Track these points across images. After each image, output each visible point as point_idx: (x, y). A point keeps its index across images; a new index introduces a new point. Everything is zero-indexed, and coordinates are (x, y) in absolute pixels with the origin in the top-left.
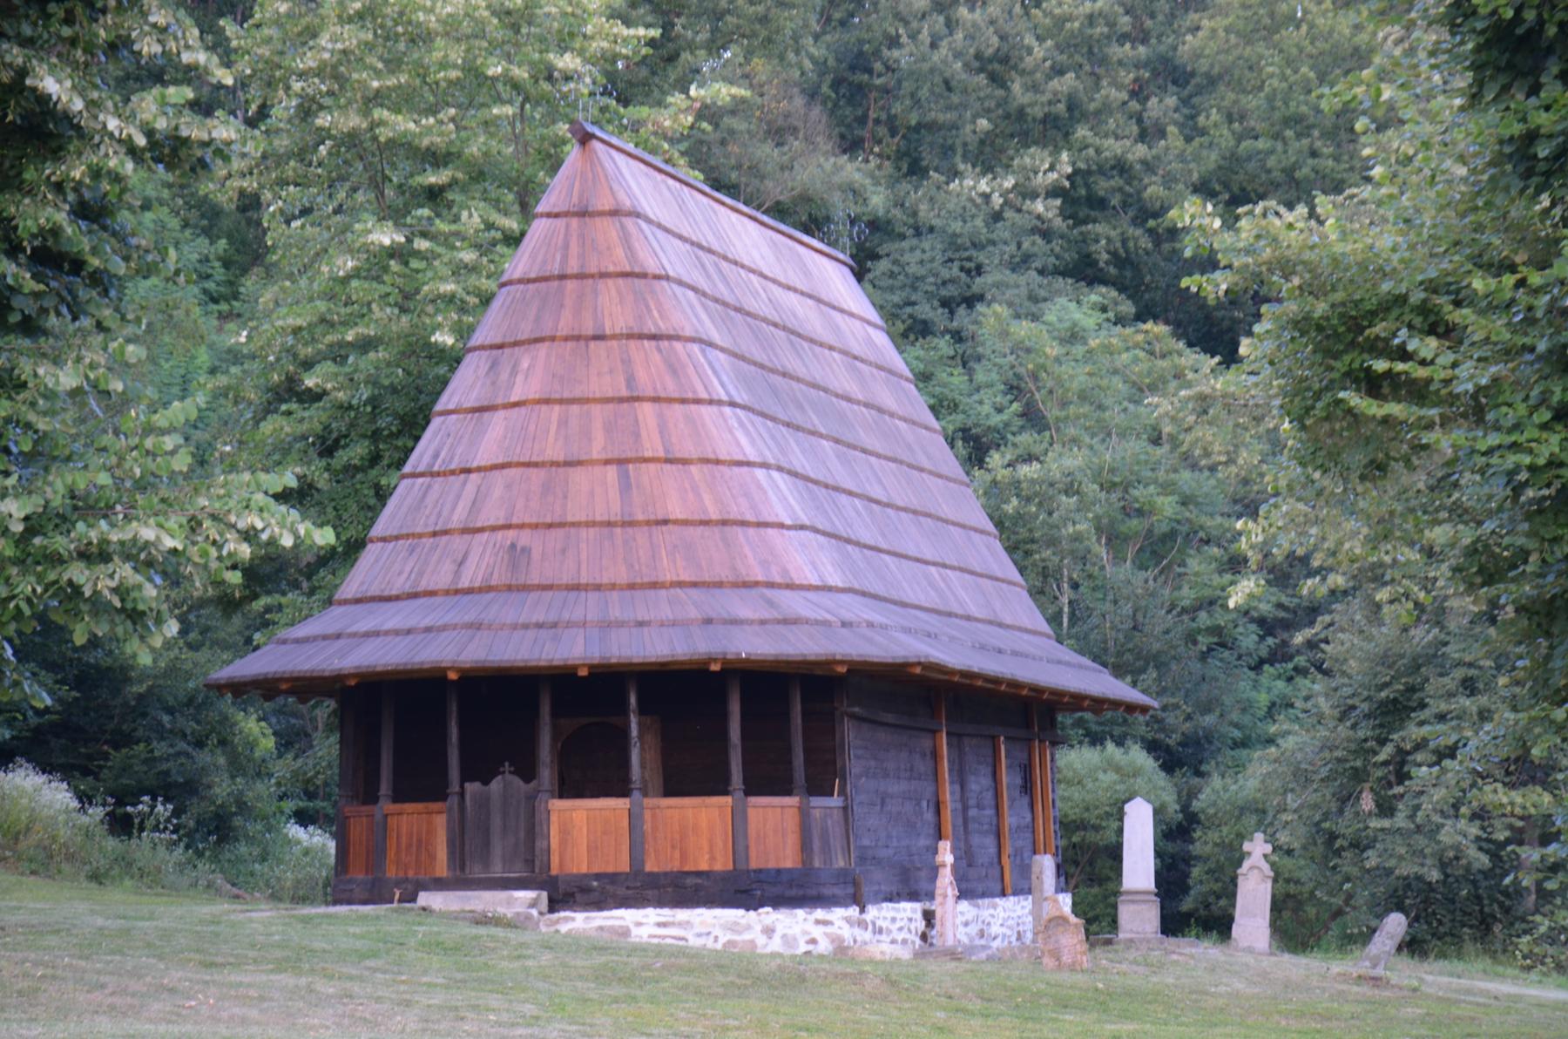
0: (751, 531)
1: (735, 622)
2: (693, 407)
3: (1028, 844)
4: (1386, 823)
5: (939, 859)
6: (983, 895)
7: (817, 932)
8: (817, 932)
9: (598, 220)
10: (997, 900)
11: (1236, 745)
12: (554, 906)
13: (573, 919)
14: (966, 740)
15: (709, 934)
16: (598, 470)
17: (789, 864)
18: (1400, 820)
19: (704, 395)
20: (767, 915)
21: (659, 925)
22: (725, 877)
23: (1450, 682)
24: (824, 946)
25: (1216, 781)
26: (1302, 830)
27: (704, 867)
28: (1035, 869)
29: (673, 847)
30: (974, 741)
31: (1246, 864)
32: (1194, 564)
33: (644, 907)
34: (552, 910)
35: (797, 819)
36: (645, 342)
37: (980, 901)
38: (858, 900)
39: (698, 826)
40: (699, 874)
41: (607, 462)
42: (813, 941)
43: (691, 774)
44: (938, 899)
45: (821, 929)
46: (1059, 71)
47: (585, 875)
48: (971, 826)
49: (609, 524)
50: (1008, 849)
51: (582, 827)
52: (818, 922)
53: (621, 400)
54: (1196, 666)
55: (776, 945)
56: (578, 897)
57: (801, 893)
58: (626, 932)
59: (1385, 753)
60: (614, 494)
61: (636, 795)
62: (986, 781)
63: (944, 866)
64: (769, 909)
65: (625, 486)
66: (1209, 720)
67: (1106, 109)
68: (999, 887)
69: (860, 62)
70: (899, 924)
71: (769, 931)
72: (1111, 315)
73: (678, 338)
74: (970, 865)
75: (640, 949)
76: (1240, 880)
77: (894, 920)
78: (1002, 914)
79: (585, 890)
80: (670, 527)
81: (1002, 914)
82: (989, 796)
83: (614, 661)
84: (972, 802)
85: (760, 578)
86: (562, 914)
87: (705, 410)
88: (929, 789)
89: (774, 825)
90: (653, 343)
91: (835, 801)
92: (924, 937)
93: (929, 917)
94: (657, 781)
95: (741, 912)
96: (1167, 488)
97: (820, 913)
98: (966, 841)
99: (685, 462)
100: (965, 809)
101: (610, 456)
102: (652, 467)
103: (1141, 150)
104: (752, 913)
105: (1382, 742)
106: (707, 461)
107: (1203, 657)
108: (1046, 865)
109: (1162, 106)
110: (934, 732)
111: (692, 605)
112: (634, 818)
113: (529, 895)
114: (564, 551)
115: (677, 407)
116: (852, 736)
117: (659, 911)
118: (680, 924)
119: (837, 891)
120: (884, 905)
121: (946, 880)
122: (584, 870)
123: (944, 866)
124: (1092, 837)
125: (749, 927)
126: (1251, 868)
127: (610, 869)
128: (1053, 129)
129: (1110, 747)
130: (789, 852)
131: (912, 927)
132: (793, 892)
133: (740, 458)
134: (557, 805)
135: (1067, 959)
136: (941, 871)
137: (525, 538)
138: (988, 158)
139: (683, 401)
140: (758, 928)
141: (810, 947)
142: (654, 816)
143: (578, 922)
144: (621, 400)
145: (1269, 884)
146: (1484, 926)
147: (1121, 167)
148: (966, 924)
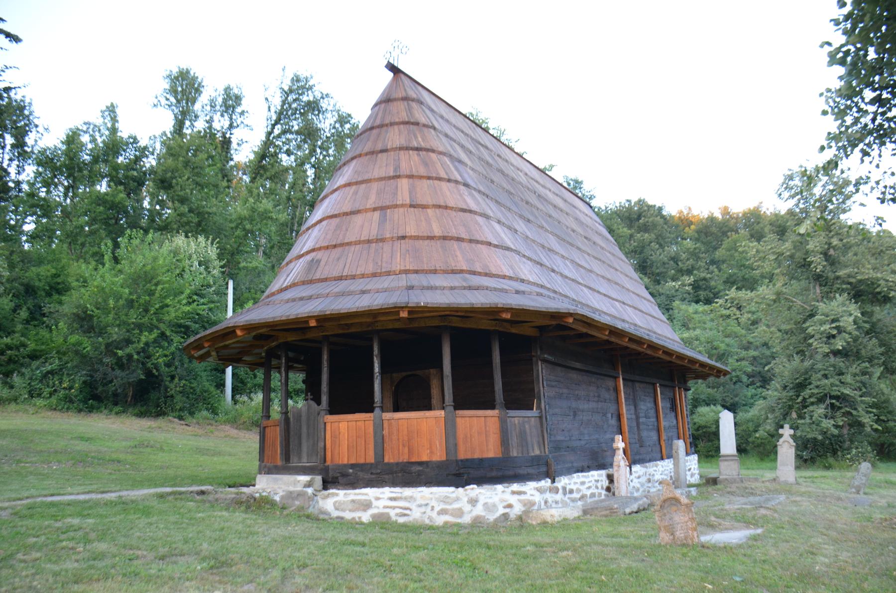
0: (465, 245)
1: (431, 288)
2: (436, 182)
3: (675, 434)
4: (803, 421)
5: (615, 445)
6: (650, 461)
7: (513, 500)
8: (513, 500)
9: (395, 103)
10: (658, 462)
11: (744, 405)
12: (327, 484)
13: (337, 495)
14: (637, 385)
15: (427, 505)
16: (369, 214)
17: (491, 455)
18: (808, 421)
19: (443, 174)
20: (473, 490)
21: (391, 499)
22: (440, 465)
23: (819, 375)
25: (741, 414)
26: (773, 425)
27: (425, 458)
28: (674, 447)
29: (404, 446)
30: (642, 385)
31: (781, 440)
32: (730, 360)
33: (383, 487)
34: (325, 488)
35: (497, 425)
36: (411, 152)
37: (647, 464)
38: (552, 475)
39: (423, 430)
40: (420, 463)
41: (375, 209)
42: (510, 506)
43: (411, 396)
44: (615, 468)
45: (517, 497)
46: (688, 259)
47: (345, 466)
48: (641, 427)
49: (369, 242)
50: (664, 436)
52: (513, 493)
53: (390, 178)
54: (732, 386)
55: (479, 510)
56: (341, 480)
57: (500, 474)
58: (367, 505)
59: (799, 400)
60: (375, 225)
61: (377, 411)
62: (650, 405)
63: (619, 449)
64: (475, 486)
65: (383, 221)
66: (737, 399)
67: (700, 267)
68: (659, 455)
69: (645, 261)
70: (587, 485)
71: (473, 502)
73: (433, 151)
74: (641, 446)
76: (779, 447)
77: (583, 483)
78: (661, 469)
79: (345, 475)
80: (407, 240)
81: (661, 469)
82: (652, 413)
83: (328, 313)
84: (642, 415)
85: (464, 268)
86: (331, 491)
87: (444, 185)
88: (612, 408)
89: (481, 430)
90: (416, 152)
91: (535, 412)
92: (608, 489)
93: (610, 478)
94: (389, 403)
95: (452, 489)
96: (722, 342)
97: (515, 487)
98: (639, 434)
99: (424, 207)
100: (638, 418)
101: (377, 205)
102: (401, 210)
103: (709, 276)
104: (460, 489)
105: (798, 396)
106: (440, 207)
107: (735, 383)
108: (680, 445)
109: (713, 268)
110: (616, 378)
112: (379, 427)
113: (304, 478)
114: (338, 259)
115: (426, 183)
116: (542, 371)
117: (393, 489)
118: (406, 499)
119: (530, 471)
120: (575, 475)
121: (620, 459)
122: (345, 462)
123: (619, 449)
124: (709, 430)
125: (457, 499)
126: (784, 442)
127: (362, 461)
128: (689, 272)
129: (712, 406)
130: (491, 447)
131: (599, 485)
132: (494, 474)
133: (465, 207)
134: (330, 418)
135: (680, 534)
136: (617, 452)
138: (673, 280)
139: (429, 178)
140: (466, 499)
141: (507, 510)
142: (390, 425)
143: (337, 502)
144: (390, 178)
145: (793, 450)
146: (834, 453)
147: (705, 279)
148: (639, 477)
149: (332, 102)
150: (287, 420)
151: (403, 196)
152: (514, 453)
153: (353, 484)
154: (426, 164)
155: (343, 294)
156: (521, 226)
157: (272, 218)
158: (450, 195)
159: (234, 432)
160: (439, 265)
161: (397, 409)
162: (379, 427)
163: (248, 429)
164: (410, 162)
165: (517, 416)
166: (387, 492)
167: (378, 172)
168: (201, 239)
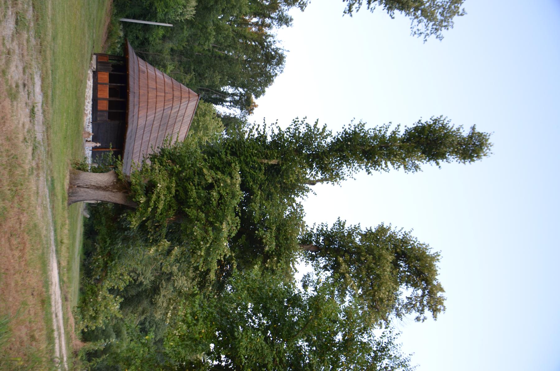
1: (134, 97)
7: (88, 112)
8: (88, 112)
12: (93, 71)
20: (91, 103)
22: (97, 96)
24: (86, 112)
39: (104, 93)
43: (112, 92)
51: (104, 77)
55: (87, 104)
58: (89, 80)
72: (189, 39)
75: (86, 83)
89: (104, 106)
93: (90, 141)
111: (136, 102)
112: (106, 84)
113: (95, 67)
121: (94, 144)
137: (146, 74)
143: (91, 75)
149: (278, 73)
150: (108, 63)
151: (159, 94)
152: (98, 113)
153: (94, 77)
154: (168, 100)
155: (134, 79)
156: (156, 124)
157: (206, 42)
158: (160, 105)
159: (107, 24)
160: (141, 100)
161: (109, 89)
162: (106, 84)
163: (108, 29)
164: (169, 96)
165: (106, 114)
166: (92, 84)
167: (167, 89)
168: (194, 12)
